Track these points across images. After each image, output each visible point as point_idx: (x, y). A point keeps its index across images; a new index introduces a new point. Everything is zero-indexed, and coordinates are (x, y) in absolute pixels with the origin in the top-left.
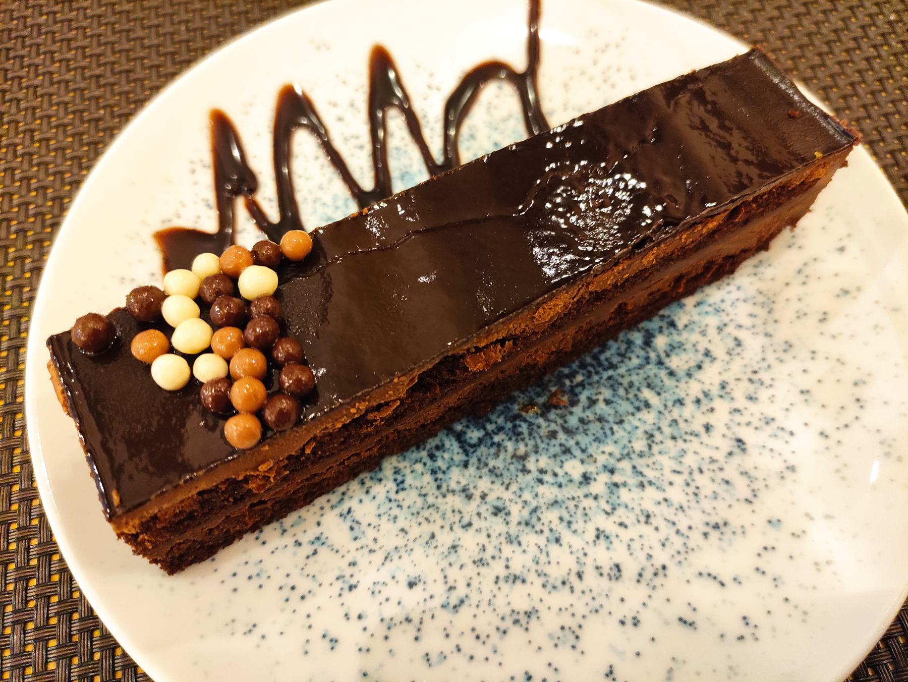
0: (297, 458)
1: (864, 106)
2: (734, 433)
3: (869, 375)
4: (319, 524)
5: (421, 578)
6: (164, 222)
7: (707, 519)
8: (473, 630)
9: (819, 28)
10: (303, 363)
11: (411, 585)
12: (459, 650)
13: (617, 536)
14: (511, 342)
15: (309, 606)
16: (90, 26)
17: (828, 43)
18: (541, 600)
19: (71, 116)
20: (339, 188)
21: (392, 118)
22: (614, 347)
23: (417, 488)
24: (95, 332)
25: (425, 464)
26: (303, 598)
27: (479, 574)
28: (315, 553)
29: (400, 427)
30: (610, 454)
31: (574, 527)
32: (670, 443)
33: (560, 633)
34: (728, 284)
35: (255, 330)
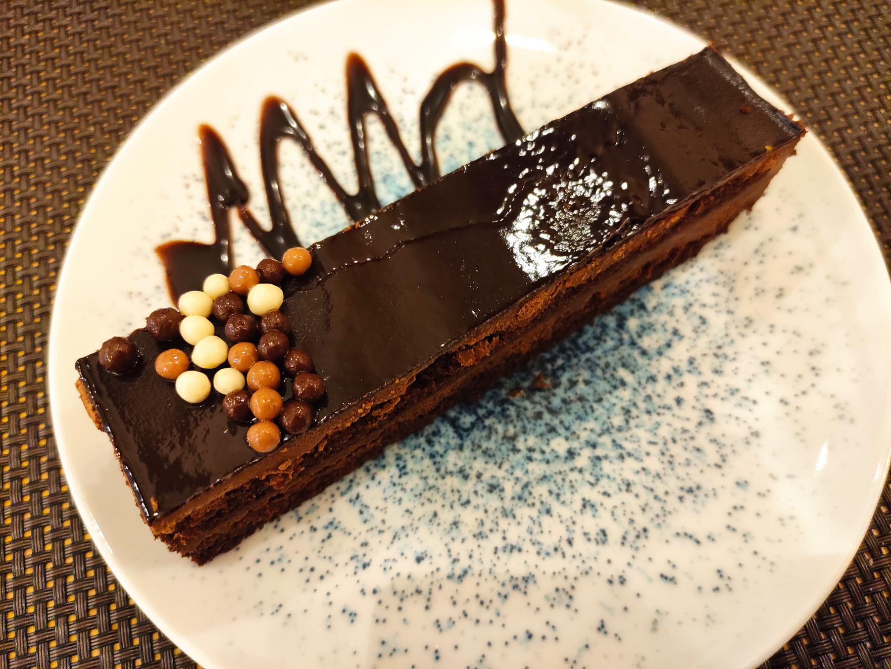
0: (312, 455)
1: (813, 87)
2: (702, 404)
3: (823, 345)
4: (331, 510)
5: (428, 553)
6: (164, 236)
7: (682, 484)
8: (477, 596)
9: (767, 12)
10: (312, 370)
11: (419, 560)
12: (466, 615)
13: (602, 504)
14: (498, 338)
15: (327, 585)
16: (72, 44)
17: (777, 26)
18: (537, 566)
19: (62, 135)
20: (326, 193)
21: (371, 123)
22: (590, 332)
23: (418, 472)
24: (120, 355)
25: (424, 450)
26: (322, 578)
27: (479, 546)
28: (329, 536)
29: (400, 419)
30: (592, 430)
31: (562, 498)
32: (645, 417)
33: (554, 594)
34: (692, 266)
35: (268, 344)
